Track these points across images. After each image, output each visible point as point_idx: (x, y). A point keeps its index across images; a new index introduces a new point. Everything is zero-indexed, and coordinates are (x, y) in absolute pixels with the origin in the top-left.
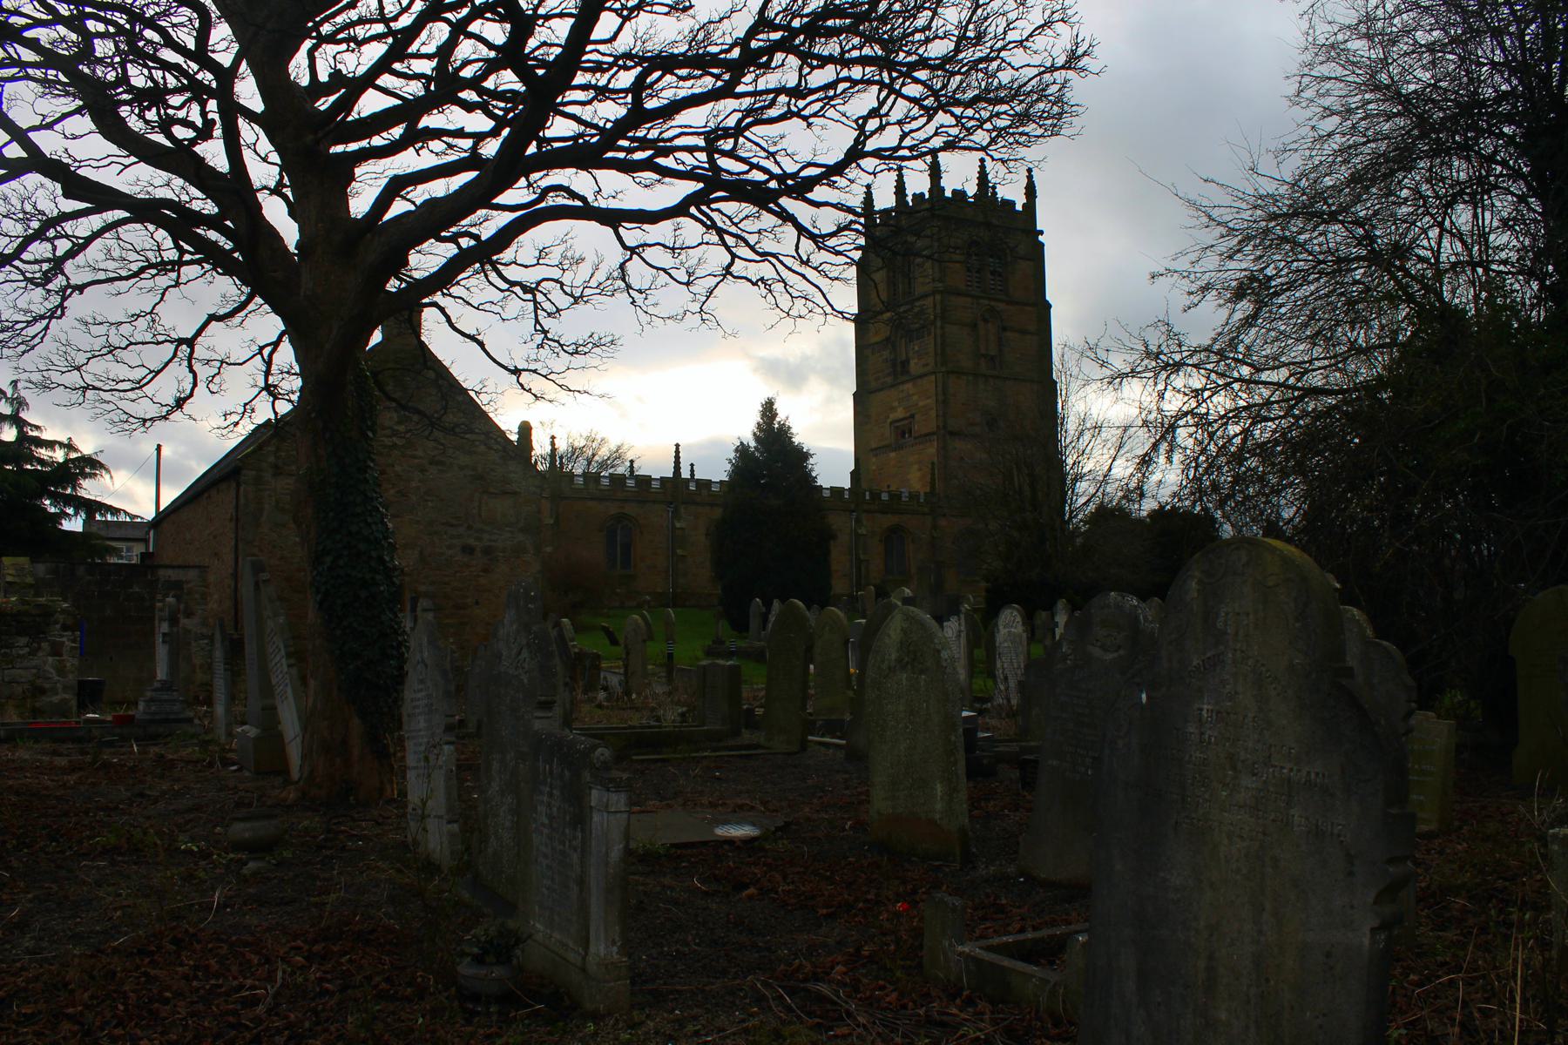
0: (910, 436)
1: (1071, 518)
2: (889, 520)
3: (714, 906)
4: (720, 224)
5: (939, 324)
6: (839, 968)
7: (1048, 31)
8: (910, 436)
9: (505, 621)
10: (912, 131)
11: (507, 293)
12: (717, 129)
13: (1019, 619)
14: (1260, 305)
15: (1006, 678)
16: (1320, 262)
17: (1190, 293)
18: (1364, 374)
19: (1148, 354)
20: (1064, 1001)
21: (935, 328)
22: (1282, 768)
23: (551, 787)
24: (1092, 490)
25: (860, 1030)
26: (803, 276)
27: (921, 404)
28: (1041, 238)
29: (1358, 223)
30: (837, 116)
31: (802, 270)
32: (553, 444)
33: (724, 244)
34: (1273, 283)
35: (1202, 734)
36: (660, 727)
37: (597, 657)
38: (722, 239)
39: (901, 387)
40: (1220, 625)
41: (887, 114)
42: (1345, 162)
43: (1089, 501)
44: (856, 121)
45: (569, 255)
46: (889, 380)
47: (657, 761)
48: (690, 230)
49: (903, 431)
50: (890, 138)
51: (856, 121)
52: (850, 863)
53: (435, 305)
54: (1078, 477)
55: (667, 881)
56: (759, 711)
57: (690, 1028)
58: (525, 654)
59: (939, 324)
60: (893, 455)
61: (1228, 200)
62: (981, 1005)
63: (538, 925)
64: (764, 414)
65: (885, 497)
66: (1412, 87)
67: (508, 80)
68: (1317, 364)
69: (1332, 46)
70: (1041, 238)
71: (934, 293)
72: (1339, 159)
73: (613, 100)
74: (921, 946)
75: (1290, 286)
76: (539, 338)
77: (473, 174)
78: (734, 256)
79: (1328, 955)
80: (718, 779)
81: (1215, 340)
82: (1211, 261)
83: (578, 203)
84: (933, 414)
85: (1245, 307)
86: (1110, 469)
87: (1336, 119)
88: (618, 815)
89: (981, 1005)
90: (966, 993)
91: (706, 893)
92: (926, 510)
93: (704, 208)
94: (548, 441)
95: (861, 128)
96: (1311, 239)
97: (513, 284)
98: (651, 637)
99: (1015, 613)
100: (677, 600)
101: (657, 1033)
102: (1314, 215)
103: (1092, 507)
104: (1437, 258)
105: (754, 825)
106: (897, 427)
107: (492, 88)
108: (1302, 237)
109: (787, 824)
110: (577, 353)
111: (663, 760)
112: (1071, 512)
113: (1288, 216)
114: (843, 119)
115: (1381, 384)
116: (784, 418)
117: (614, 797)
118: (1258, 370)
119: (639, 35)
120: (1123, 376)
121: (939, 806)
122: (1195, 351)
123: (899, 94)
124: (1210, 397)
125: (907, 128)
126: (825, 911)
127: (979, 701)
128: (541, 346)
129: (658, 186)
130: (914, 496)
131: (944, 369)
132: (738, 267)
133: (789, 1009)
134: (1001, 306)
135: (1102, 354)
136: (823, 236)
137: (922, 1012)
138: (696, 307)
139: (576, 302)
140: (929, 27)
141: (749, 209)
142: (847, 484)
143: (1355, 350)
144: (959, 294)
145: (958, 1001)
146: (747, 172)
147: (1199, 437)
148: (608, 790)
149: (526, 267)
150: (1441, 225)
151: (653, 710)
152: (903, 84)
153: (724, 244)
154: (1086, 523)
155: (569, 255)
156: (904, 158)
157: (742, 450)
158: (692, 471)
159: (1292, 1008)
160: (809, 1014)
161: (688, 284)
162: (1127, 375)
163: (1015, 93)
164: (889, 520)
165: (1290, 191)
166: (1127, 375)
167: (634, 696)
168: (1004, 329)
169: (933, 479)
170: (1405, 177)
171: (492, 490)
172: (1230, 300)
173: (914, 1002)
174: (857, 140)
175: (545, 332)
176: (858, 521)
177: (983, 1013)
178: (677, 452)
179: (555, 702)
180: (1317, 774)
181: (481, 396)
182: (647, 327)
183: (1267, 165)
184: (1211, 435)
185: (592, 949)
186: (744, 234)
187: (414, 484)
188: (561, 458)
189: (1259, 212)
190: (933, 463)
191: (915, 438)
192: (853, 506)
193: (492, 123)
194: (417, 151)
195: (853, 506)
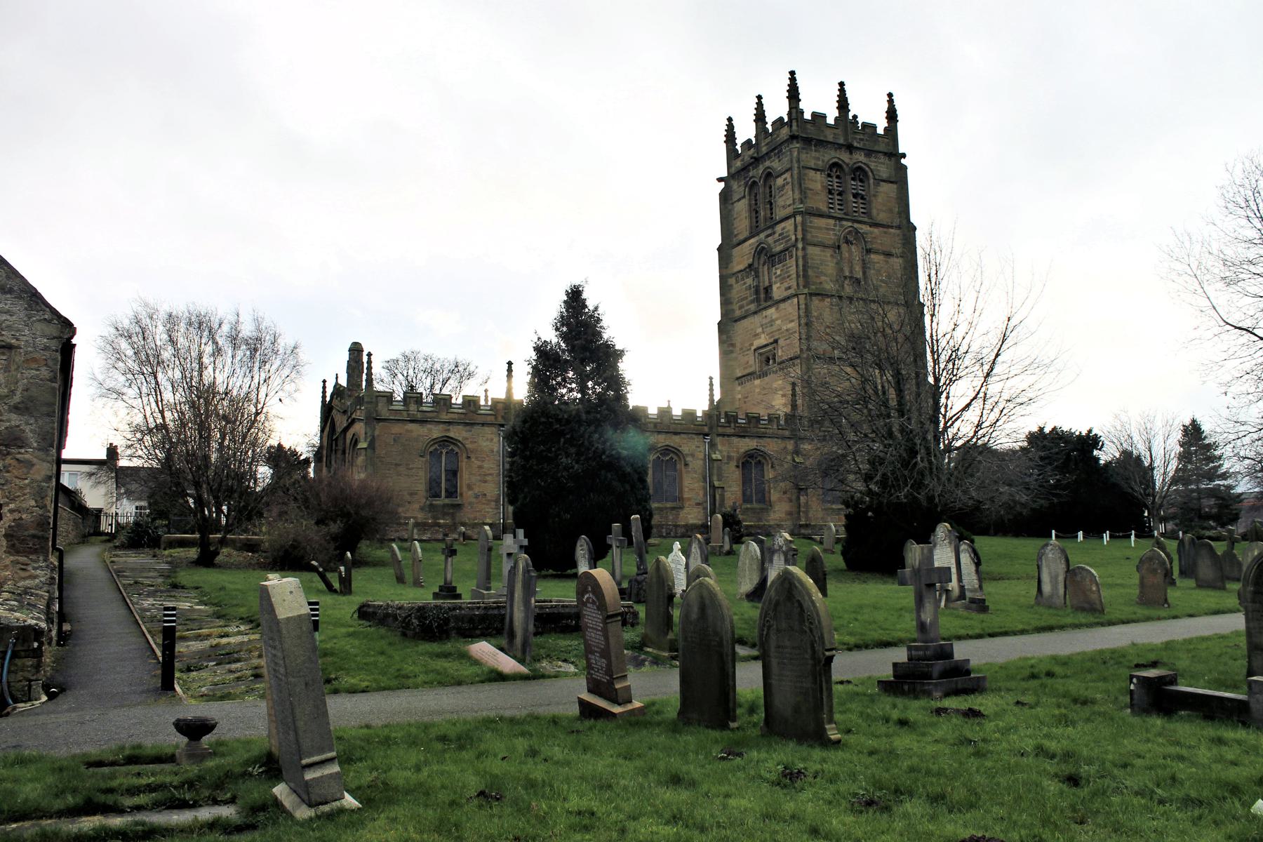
0: (774, 362)
1: (946, 428)
2: (748, 444)
5: (800, 245)
8: (774, 362)
21: (797, 249)
28: (903, 161)
39: (764, 313)
49: (767, 357)
59: (800, 245)
60: (757, 382)
70: (903, 161)
71: (794, 215)
92: (787, 433)
106: (761, 354)
130: (771, 419)
131: (806, 291)
134: (864, 228)
144: (821, 215)
164: (748, 444)
168: (869, 251)
176: (712, 445)
192: (706, 429)
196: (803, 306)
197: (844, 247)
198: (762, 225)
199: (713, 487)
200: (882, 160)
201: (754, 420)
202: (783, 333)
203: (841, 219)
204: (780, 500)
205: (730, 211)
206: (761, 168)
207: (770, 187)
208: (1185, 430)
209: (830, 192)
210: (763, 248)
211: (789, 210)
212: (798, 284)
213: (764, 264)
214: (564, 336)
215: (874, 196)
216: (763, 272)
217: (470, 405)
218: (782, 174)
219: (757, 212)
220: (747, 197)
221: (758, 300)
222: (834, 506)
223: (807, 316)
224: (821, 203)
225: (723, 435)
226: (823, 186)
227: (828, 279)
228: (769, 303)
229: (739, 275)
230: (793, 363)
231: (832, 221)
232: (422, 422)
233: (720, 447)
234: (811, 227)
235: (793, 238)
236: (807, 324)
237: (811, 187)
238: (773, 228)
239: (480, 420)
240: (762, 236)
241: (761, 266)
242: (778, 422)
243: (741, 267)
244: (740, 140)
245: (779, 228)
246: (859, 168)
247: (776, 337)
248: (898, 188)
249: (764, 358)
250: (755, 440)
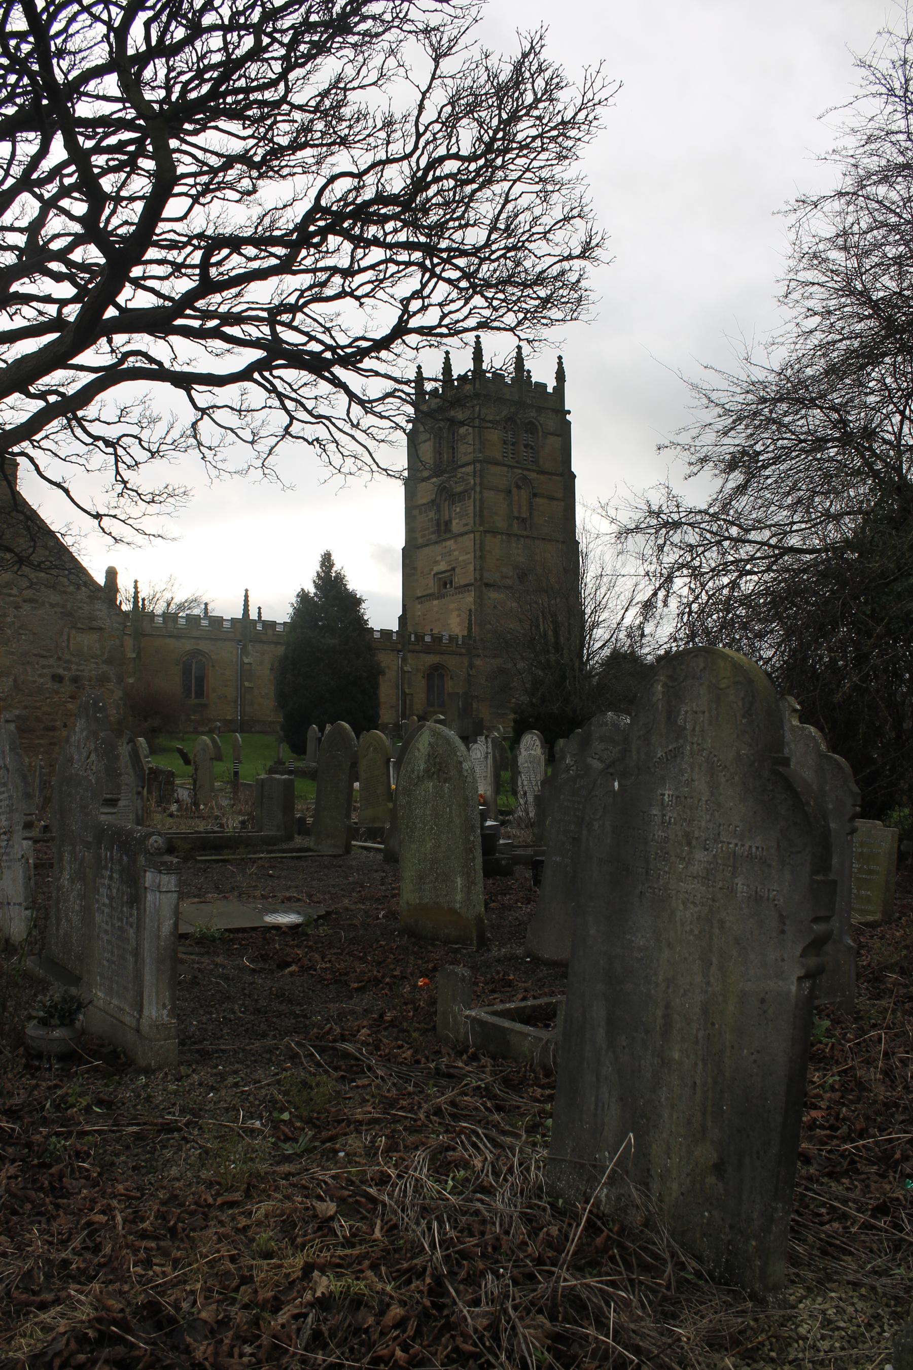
1: (588, 660)
2: (431, 659)
3: (260, 981)
4: (280, 389)
5: (478, 489)
6: (364, 1031)
7: (568, 226)
9: (77, 729)
10: (451, 312)
11: (92, 447)
12: (281, 304)
13: (538, 743)
14: (750, 476)
15: (525, 794)
16: (801, 441)
17: (691, 464)
18: (833, 533)
19: (651, 513)
20: (554, 1056)
22: (729, 843)
23: (111, 872)
24: (607, 636)
25: (379, 1081)
26: (353, 437)
27: (461, 558)
28: (568, 417)
29: (833, 408)
30: (386, 297)
31: (353, 432)
32: (136, 587)
33: (285, 408)
34: (761, 458)
35: (664, 815)
36: (222, 832)
37: (172, 774)
38: (282, 403)
39: (444, 544)
40: (680, 722)
41: (428, 297)
42: (824, 355)
43: (604, 645)
44: (401, 301)
45: (147, 414)
46: (434, 537)
47: (217, 861)
48: (255, 394)
49: (445, 582)
50: (431, 318)
51: (401, 301)
52: (381, 946)
53: (23, 454)
54: (595, 625)
55: (219, 960)
56: (310, 820)
57: (231, 1080)
58: (93, 757)
59: (478, 489)
60: (435, 602)
61: (724, 385)
62: (484, 1060)
63: (99, 994)
64: (323, 564)
65: (428, 639)
66: (881, 294)
67: (92, 254)
68: (795, 527)
69: (815, 256)
70: (568, 417)
71: (474, 462)
72: (819, 353)
73: (188, 276)
74: (435, 1013)
75: (776, 460)
76: (119, 487)
77: (56, 335)
78: (292, 418)
79: (763, 1001)
80: (271, 876)
81: (710, 506)
82: (709, 437)
83: (154, 366)
84: (471, 567)
85: (737, 478)
86: (623, 618)
87: (818, 319)
88: (169, 895)
89: (484, 1060)
90: (471, 1050)
91: (254, 970)
92: (463, 651)
93: (266, 374)
94: (133, 585)
95: (405, 310)
96: (794, 421)
97: (97, 438)
98: (219, 758)
99: (535, 738)
100: (244, 727)
101: (200, 1084)
102: (798, 400)
103: (607, 652)
104: (899, 442)
105: (299, 913)
107: (80, 261)
108: (787, 420)
109: (328, 913)
110: (153, 501)
111: (224, 861)
112: (589, 655)
113: (776, 401)
114: (392, 301)
115: (848, 544)
117: (165, 878)
118: (747, 531)
119: (211, 218)
120: (629, 531)
121: (459, 897)
122: (691, 512)
123: (440, 278)
124: (703, 553)
125: (447, 309)
126: (356, 985)
127: (504, 814)
128: (121, 495)
129: (228, 355)
130: (452, 639)
131: (481, 529)
132: (296, 428)
133: (318, 1065)
134: (533, 475)
135: (612, 513)
136: (370, 402)
137: (432, 1065)
138: (259, 463)
139: (153, 457)
140: (462, 217)
141: (305, 376)
142: (395, 627)
143: (828, 516)
144: (497, 463)
145: (465, 1057)
146: (305, 344)
147: (693, 586)
148: (160, 872)
149: (108, 424)
150: (902, 413)
151: (217, 818)
152: (443, 270)
153: (285, 408)
154: (602, 665)
155: (147, 414)
156: (442, 335)
157: (303, 596)
158: (260, 613)
159: (732, 1047)
160: (336, 1069)
161: (252, 443)
162: (632, 531)
163: (540, 280)
164: (431, 659)
165: (777, 379)
166: (632, 531)
167: (202, 807)
168: (535, 495)
169: (470, 624)
170: (873, 370)
171: (79, 625)
172: (723, 471)
173: (427, 1058)
174: (401, 318)
175: (125, 482)
176: (404, 660)
177: (484, 1067)
178: (246, 596)
179: (119, 800)
180: (757, 848)
181: (66, 538)
182: (216, 481)
183: (759, 356)
184: (703, 585)
185: (146, 1013)
186: (303, 400)
187: (9, 619)
188: (144, 600)
189: (750, 397)
190: (470, 611)
192: (400, 646)
193: (75, 291)
194: (11, 316)
196: (478, 542)
197: (514, 490)
199: (404, 693)
203: (513, 467)
209: (505, 443)
211: (469, 458)
214: (317, 586)
221: (438, 531)
223: (481, 550)
225: (413, 652)
228: (448, 536)
231: (505, 469)
232: (178, 637)
236: (481, 557)
243: (424, 501)
246: (531, 422)
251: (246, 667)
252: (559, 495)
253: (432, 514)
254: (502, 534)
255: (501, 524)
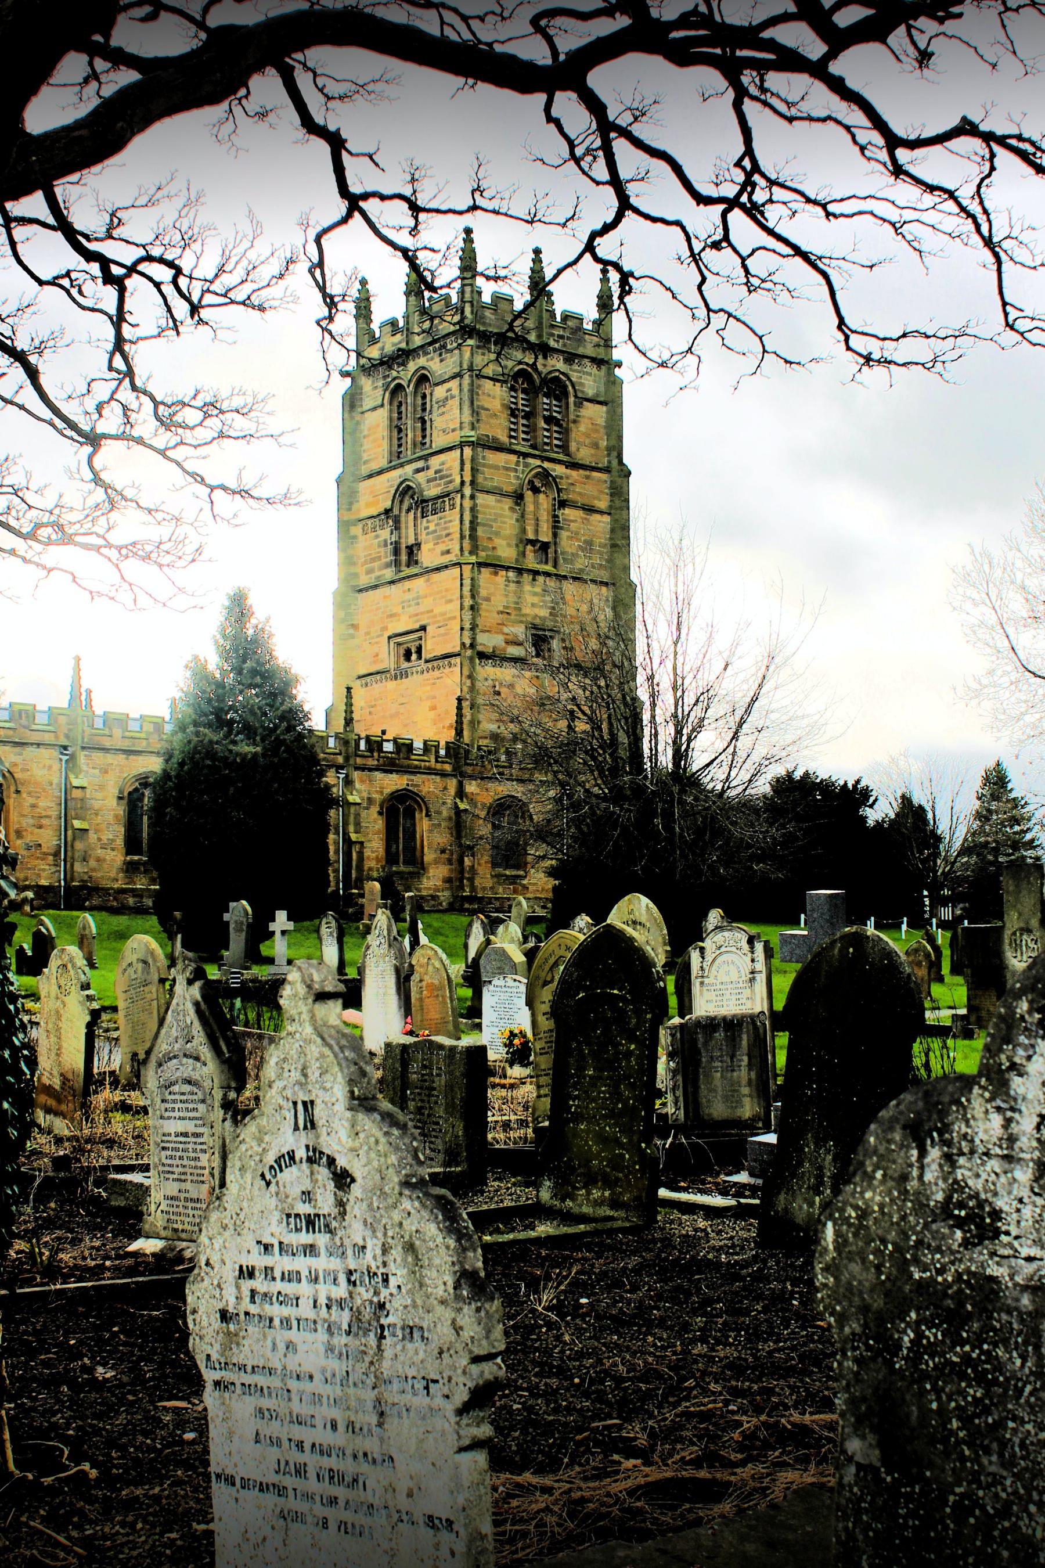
0: (420, 657)
2: (393, 782)
5: (467, 491)
8: (420, 657)
21: (462, 497)
28: (617, 371)
46: (389, 574)
59: (467, 491)
65: (388, 747)
71: (461, 445)
92: (448, 768)
106: (399, 644)
116: (262, 619)
131: (473, 559)
134: (558, 470)
144: (500, 448)
164: (393, 782)
168: (563, 504)
191: (427, 661)
195: (340, 760)
196: (467, 582)
197: (529, 495)
198: (409, 455)
200: (588, 369)
201: (404, 749)
202: (435, 616)
203: (525, 455)
204: (436, 862)
205: (358, 423)
206: (412, 366)
207: (424, 397)
208: (987, 780)
209: (513, 413)
210: (409, 487)
211: (454, 438)
212: (462, 549)
213: (408, 510)
214: (225, 655)
215: (575, 422)
216: (407, 522)
217: (20, 717)
218: (444, 382)
219: (400, 431)
220: (387, 406)
222: (508, 872)
223: (473, 597)
224: (498, 428)
226: (503, 405)
227: (504, 543)
228: (414, 570)
229: (369, 522)
230: (450, 664)
231: (513, 458)
233: (357, 785)
234: (484, 465)
235: (458, 480)
236: (472, 608)
237: (486, 406)
238: (426, 460)
239: (35, 738)
240: (409, 469)
241: (403, 514)
242: (437, 752)
244: (380, 315)
245: (435, 462)
247: (423, 623)
248: (608, 412)
249: (402, 652)
250: (406, 777)
251: (77, 794)
252: (603, 504)
253: (385, 534)
254: (507, 568)
255: (507, 552)
